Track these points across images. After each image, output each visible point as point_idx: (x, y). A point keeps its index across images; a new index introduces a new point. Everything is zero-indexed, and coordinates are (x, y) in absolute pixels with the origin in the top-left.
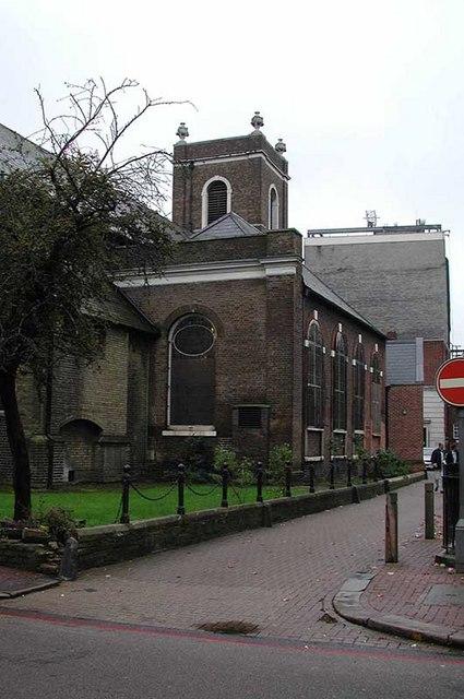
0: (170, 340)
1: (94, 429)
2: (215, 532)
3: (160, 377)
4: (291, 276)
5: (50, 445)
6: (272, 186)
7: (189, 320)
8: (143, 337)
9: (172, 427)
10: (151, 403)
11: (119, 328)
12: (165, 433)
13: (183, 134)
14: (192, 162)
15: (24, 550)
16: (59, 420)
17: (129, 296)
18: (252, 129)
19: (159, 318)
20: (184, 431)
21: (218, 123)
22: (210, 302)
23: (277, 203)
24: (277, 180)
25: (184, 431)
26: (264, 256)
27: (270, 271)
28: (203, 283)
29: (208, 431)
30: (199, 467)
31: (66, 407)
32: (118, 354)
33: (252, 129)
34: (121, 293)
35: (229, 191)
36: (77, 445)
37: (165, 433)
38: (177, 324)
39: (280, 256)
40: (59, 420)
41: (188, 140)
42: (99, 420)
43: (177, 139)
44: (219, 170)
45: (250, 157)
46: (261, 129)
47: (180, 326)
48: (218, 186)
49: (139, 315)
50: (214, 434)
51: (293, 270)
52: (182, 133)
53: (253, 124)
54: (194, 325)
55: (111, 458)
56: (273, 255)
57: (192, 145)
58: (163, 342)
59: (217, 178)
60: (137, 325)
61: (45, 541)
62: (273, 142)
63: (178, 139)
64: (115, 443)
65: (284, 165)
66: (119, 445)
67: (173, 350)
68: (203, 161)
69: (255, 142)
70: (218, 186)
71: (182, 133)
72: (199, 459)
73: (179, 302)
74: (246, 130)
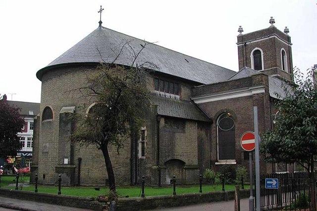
0: (217, 124)
1: (181, 163)
2: (194, 203)
3: (214, 140)
4: (263, 93)
5: (159, 170)
6: (282, 49)
7: (224, 115)
8: (204, 123)
9: (219, 161)
10: (211, 151)
11: (191, 121)
12: (216, 163)
13: (273, 22)
14: (246, 43)
15: (99, 204)
16: (163, 160)
17: (200, 107)
18: (270, 25)
19: (212, 114)
20: (223, 162)
21: (275, 21)
22: (232, 107)
23: (286, 57)
24: (285, 46)
25: (223, 162)
26: (251, 86)
27: (254, 92)
28: (228, 99)
29: (233, 162)
30: (229, 177)
31: (167, 154)
32: (192, 131)
33: (270, 25)
34: (196, 105)
35: (262, 53)
36: (173, 170)
37: (216, 163)
38: (219, 117)
39: (257, 85)
40: (163, 160)
41: (243, 33)
42: (183, 159)
43: (238, 33)
44: (257, 45)
45: (270, 37)
46: (274, 24)
47: (221, 118)
48: (257, 52)
49: (205, 115)
50: (235, 163)
51: (264, 91)
52: (241, 30)
53: (270, 22)
54: (226, 120)
55: (188, 175)
56: (254, 85)
57: (245, 35)
58: (214, 125)
59: (256, 49)
60: (202, 119)
61: (106, 202)
62: (281, 29)
63: (239, 33)
64: (192, 168)
65: (288, 39)
66: (193, 169)
67: (219, 128)
68: (250, 42)
69: (272, 30)
70: (257, 52)
71: (241, 30)
72: (229, 174)
73: (219, 108)
74: (267, 25)
